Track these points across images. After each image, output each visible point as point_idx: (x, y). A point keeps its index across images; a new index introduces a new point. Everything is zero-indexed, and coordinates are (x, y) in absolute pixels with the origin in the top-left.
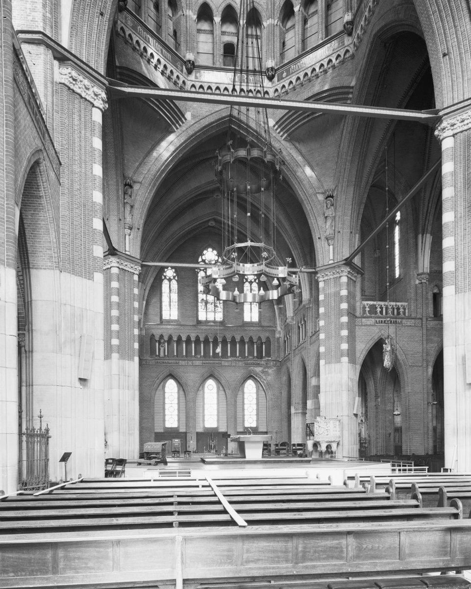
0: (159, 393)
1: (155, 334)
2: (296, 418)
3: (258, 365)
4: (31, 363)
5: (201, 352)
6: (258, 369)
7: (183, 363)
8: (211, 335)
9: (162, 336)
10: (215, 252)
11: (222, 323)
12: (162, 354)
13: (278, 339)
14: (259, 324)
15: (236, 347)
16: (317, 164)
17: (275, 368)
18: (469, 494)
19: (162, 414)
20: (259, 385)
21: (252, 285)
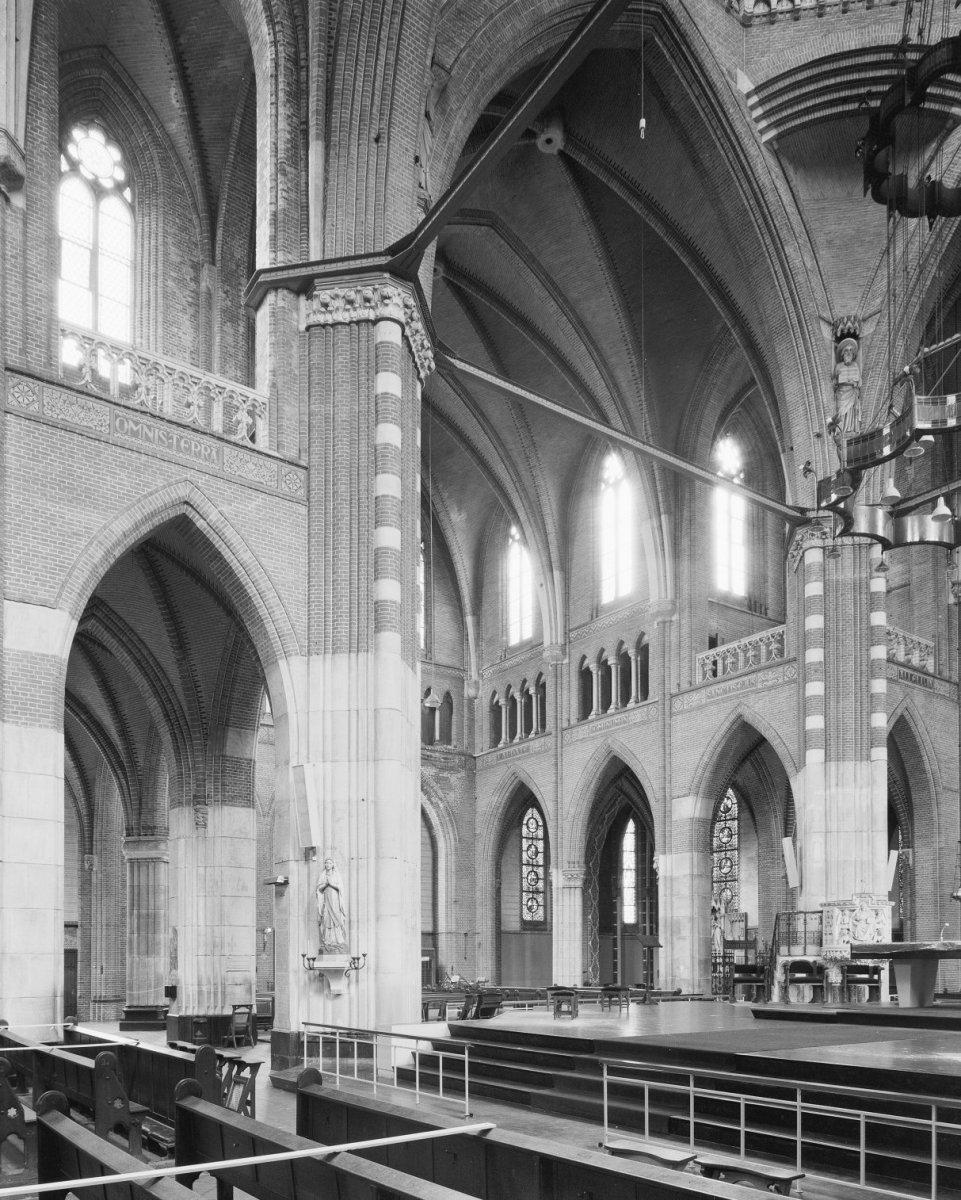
2: (566, 898)
4: (736, 143)
13: (471, 701)
16: (829, 242)
18: (957, 1015)
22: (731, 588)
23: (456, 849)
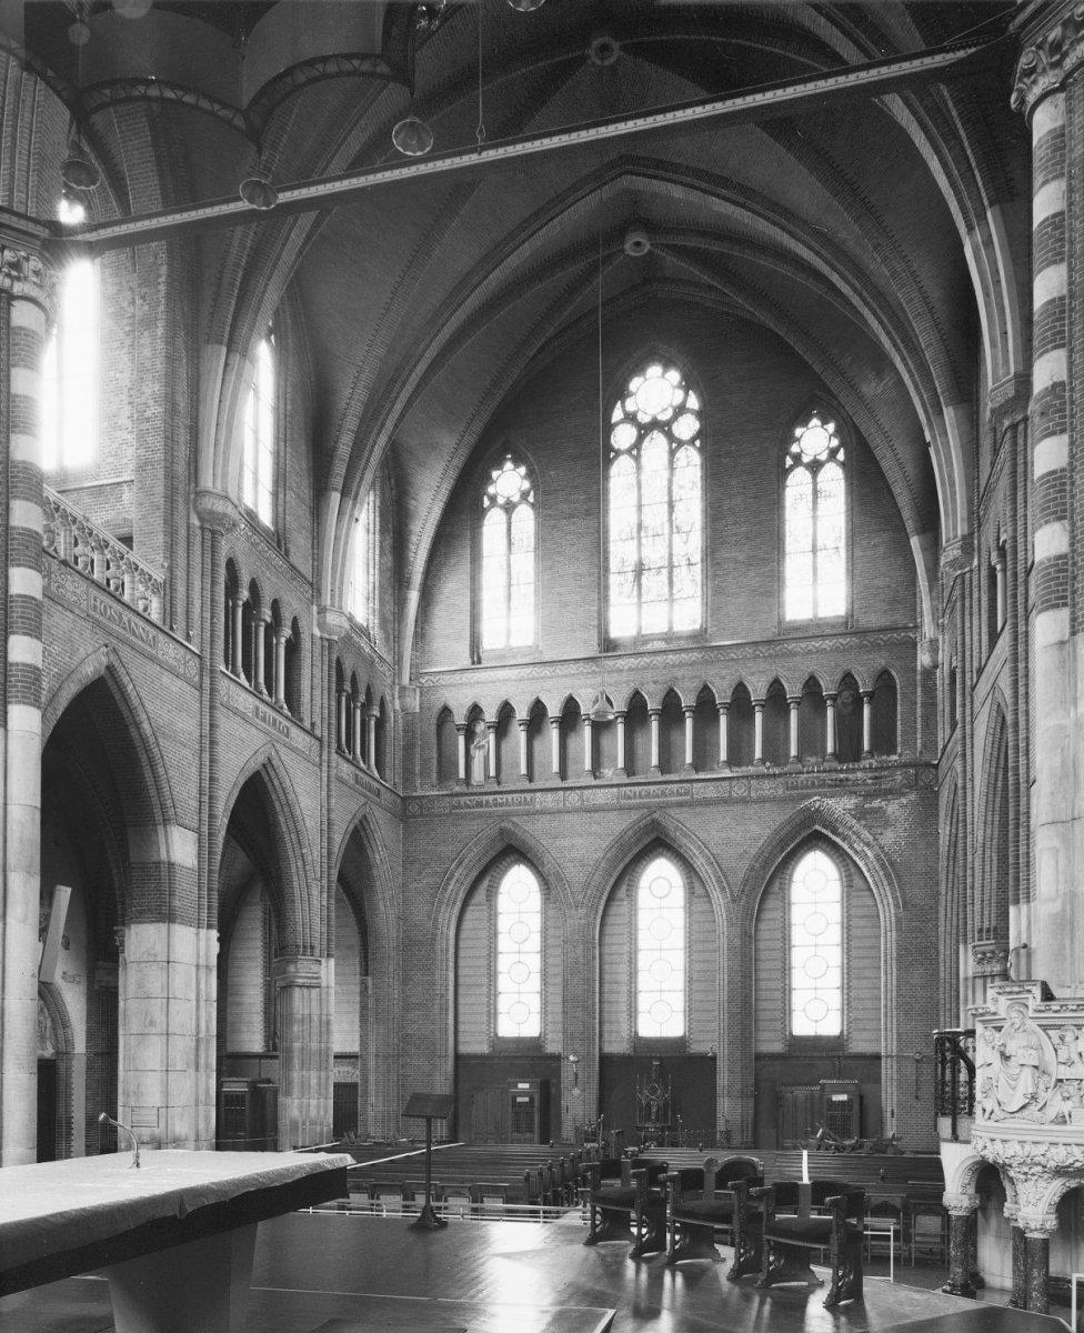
0: (477, 915)
1: (452, 705)
3: (840, 787)
5: (616, 759)
6: (840, 806)
7: (549, 800)
8: (652, 687)
9: (475, 712)
10: (674, 376)
11: (699, 638)
12: (478, 775)
14: (848, 628)
15: (825, 716)
17: (912, 797)
19: (485, 990)
20: (853, 870)
21: (822, 476)
22: (256, 505)
23: (898, 921)
